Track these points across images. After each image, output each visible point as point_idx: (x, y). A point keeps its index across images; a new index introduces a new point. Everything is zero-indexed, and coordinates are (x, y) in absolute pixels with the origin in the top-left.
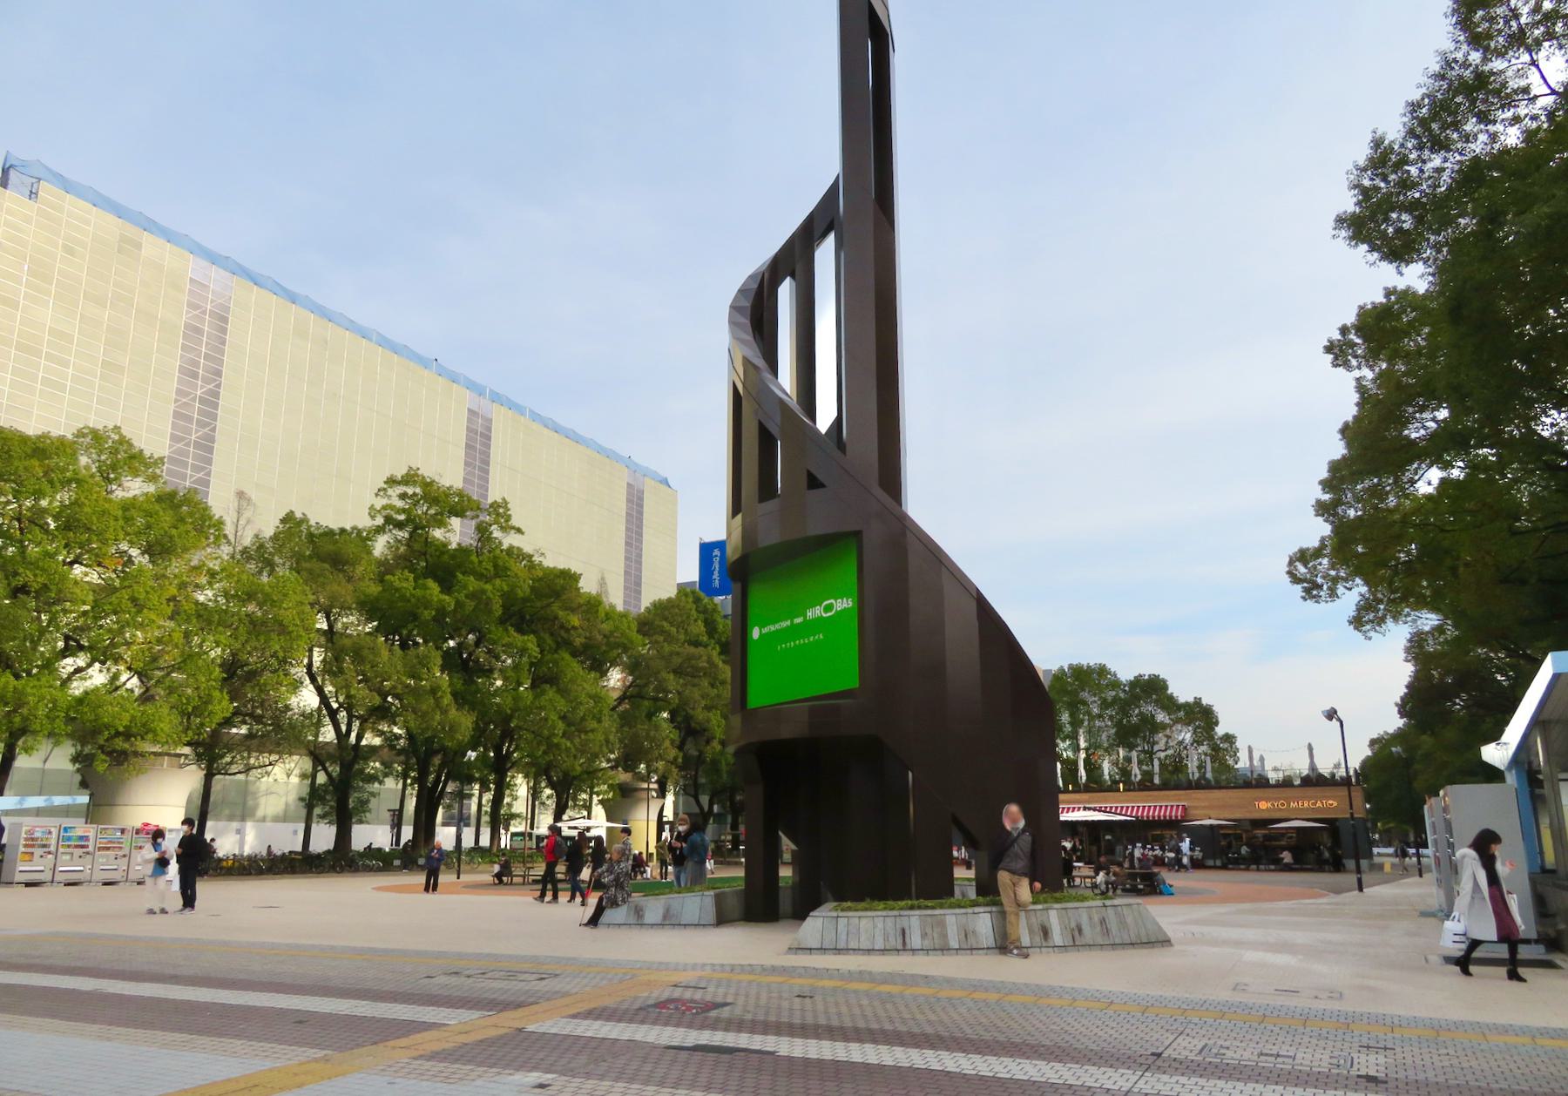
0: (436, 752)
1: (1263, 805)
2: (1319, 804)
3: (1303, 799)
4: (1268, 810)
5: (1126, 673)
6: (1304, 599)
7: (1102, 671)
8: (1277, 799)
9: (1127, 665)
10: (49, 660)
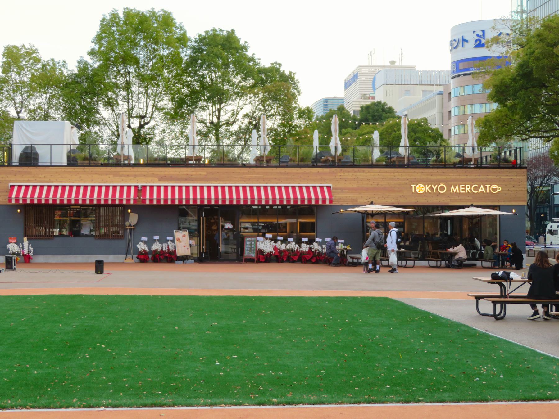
0: (234, 92)
1: (420, 189)
2: (482, 189)
3: (465, 181)
4: (425, 194)
5: (194, 25)
6: (153, 9)
7: (167, 21)
8: (438, 182)
9: (95, 29)
10: (205, 134)
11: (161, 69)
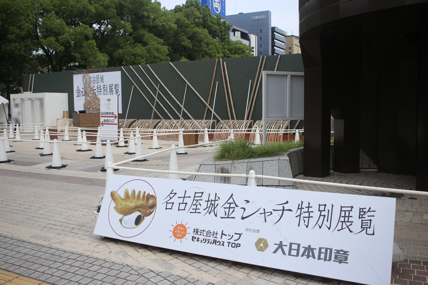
11: (302, 250)
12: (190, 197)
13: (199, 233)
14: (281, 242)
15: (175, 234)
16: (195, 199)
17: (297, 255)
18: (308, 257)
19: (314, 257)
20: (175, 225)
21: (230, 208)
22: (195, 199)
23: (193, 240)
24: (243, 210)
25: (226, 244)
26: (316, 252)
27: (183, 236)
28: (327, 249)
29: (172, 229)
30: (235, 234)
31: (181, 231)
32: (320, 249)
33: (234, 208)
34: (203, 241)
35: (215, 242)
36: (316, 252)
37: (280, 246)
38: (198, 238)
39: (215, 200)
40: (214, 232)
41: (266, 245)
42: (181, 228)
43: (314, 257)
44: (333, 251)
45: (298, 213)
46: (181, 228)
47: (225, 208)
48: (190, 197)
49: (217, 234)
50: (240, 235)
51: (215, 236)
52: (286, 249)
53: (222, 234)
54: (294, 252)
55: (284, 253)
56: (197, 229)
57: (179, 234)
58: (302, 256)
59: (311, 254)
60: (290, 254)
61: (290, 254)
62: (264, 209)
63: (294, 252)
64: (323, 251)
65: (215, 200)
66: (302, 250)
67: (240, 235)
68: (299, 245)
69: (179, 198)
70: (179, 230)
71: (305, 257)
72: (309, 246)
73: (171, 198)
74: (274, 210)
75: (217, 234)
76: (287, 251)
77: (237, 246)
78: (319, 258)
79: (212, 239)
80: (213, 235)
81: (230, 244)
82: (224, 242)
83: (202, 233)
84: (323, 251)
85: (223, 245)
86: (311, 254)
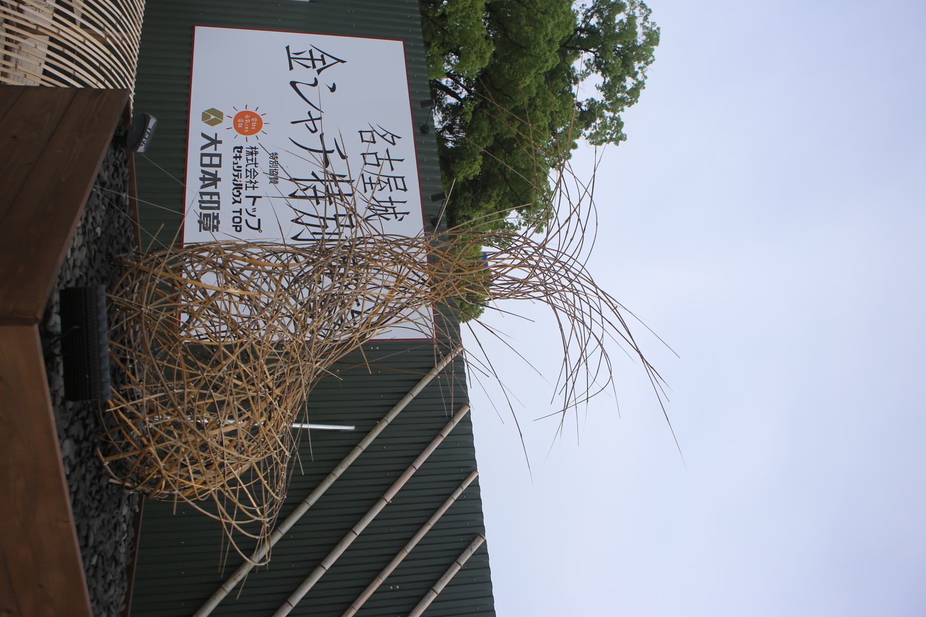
11: (212, 170)
12: (392, 169)
13: (250, 157)
14: (220, 142)
15: (241, 115)
16: (392, 180)
17: (202, 165)
18: (202, 179)
19: (203, 187)
20: (259, 113)
21: (312, 59)
22: (392, 180)
23: (235, 148)
24: (313, 82)
25: (237, 207)
26: (211, 189)
27: (241, 131)
28: (218, 202)
29: (251, 109)
30: (259, 220)
31: (250, 124)
32: (217, 194)
33: (314, 67)
34: (235, 166)
35: (238, 187)
36: (211, 189)
37: (215, 142)
38: (240, 157)
39: (395, 213)
40: (256, 182)
41: (213, 123)
42: (254, 124)
43: (203, 187)
44: (216, 212)
45: (321, 177)
46: (254, 124)
47: (311, 52)
48: (392, 169)
49: (254, 187)
50: (259, 228)
51: (249, 185)
52: (211, 150)
53: (255, 198)
54: (206, 160)
55: (203, 148)
56: (256, 153)
57: (244, 123)
58: (203, 171)
59: (206, 182)
60: (203, 155)
61: (203, 155)
62: (320, 119)
63: (206, 160)
64: (215, 198)
65: (395, 213)
66: (212, 170)
67: (259, 228)
68: (219, 166)
69: (387, 151)
70: (251, 122)
71: (202, 175)
72: (219, 180)
73: (382, 137)
74: (321, 136)
75: (254, 187)
76: (206, 151)
77: (236, 227)
78: (202, 194)
79: (243, 180)
80: (251, 182)
81: (238, 214)
82: (240, 202)
83: (250, 162)
84: (215, 198)
85: (235, 202)
86: (206, 182)
